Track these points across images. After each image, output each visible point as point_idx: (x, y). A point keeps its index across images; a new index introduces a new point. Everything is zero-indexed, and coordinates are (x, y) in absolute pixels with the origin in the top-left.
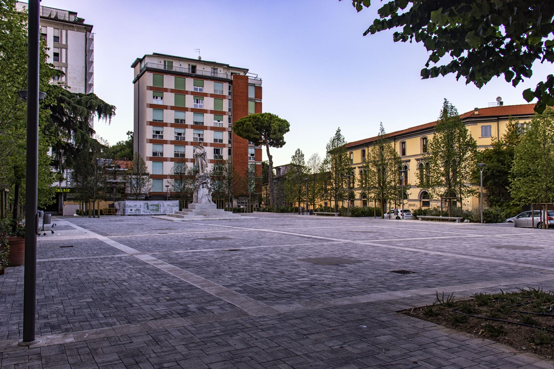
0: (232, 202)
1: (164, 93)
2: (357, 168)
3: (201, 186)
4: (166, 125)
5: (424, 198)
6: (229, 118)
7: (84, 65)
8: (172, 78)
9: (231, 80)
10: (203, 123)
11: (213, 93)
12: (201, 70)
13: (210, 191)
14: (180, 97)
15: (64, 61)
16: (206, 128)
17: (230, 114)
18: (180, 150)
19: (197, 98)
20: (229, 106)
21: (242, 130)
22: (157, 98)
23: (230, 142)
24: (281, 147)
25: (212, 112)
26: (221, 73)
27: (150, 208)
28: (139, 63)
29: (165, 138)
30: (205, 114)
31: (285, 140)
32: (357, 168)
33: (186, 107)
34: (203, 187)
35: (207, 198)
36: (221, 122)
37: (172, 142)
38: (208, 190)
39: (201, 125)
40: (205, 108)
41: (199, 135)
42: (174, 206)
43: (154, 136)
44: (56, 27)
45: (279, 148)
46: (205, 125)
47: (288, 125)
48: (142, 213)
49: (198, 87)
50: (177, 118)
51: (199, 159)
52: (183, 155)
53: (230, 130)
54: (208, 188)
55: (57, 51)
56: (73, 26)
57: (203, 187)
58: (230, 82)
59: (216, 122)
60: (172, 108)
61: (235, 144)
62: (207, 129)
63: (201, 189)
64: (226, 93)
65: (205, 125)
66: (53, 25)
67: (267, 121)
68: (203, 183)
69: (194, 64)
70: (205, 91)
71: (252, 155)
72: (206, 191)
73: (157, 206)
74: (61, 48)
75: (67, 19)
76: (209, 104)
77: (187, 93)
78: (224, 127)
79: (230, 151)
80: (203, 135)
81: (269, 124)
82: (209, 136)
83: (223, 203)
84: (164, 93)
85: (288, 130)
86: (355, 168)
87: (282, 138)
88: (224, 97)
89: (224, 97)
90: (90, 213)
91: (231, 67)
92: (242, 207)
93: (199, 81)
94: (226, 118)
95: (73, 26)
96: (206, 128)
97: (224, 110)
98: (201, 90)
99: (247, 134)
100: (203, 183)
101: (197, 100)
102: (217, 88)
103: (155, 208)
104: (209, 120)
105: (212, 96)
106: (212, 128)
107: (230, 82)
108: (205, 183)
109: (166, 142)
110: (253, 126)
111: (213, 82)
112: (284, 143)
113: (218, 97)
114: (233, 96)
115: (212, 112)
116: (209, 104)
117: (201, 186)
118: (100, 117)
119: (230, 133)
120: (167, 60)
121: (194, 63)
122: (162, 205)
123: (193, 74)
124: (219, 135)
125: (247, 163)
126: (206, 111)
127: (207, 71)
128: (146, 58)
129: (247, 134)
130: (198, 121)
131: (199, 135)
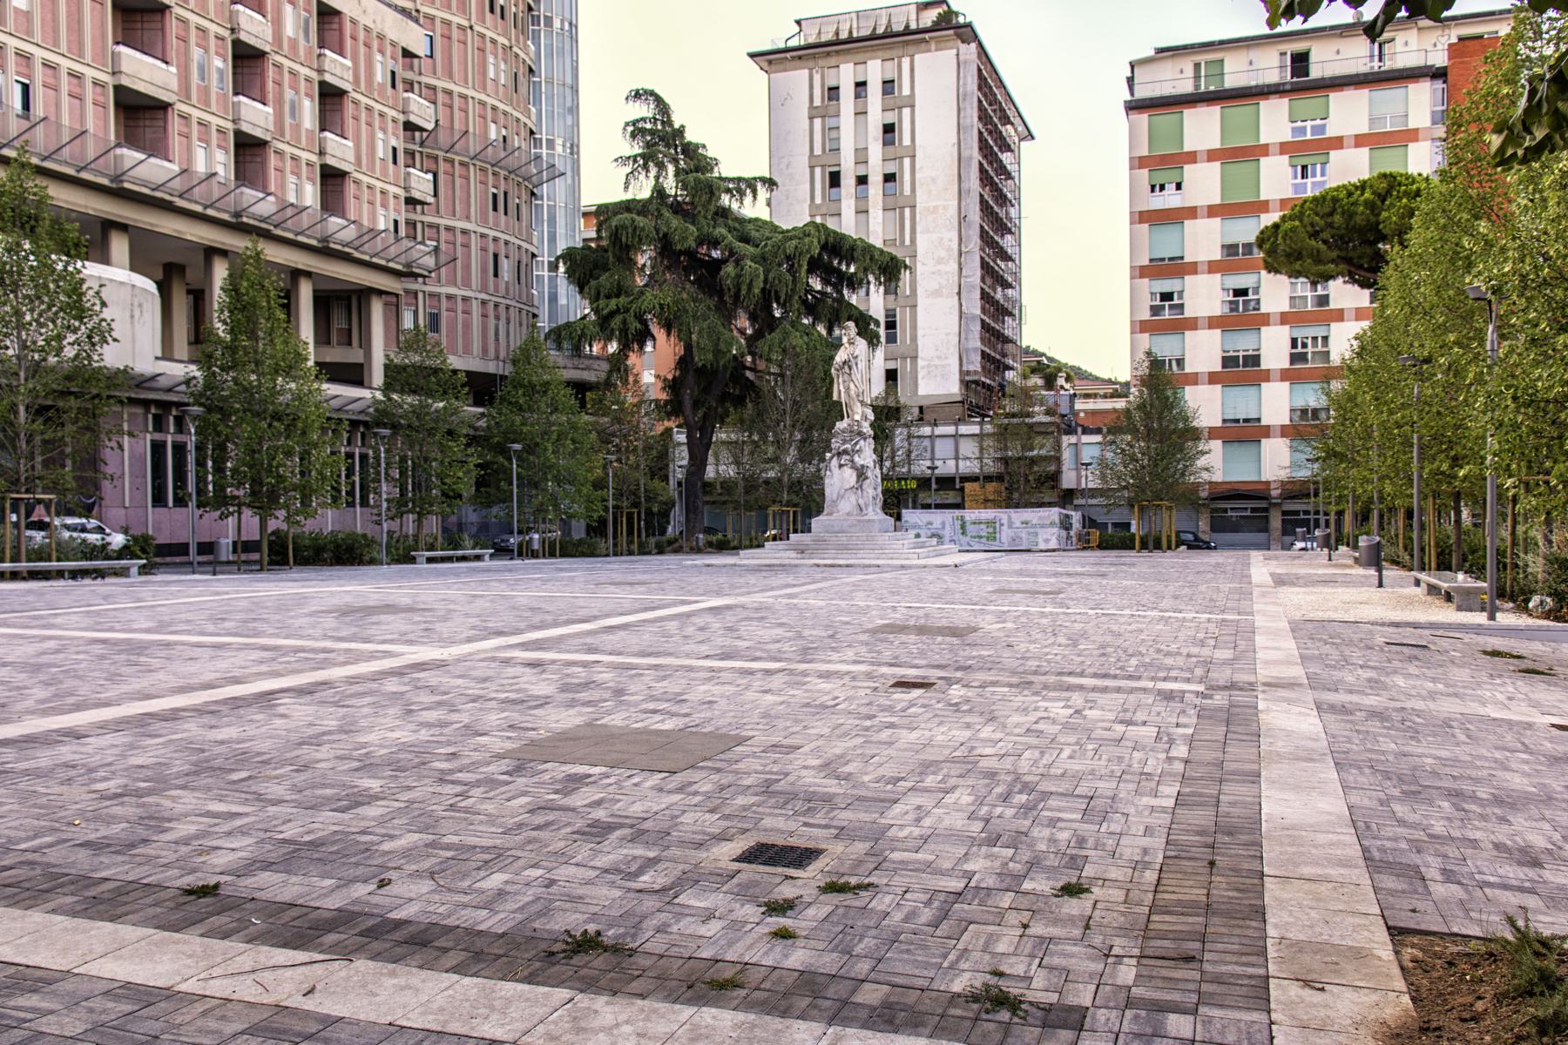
1: (1186, 167)
4: (1193, 269)
7: (955, 140)
8: (1213, 113)
14: (1241, 169)
15: (907, 141)
18: (1242, 343)
19: (1304, 161)
22: (1162, 188)
29: (1189, 313)
34: (841, 466)
35: (853, 499)
37: (1213, 323)
42: (1043, 526)
43: (1155, 310)
44: (888, 54)
50: (1229, 241)
52: (1254, 360)
55: (891, 118)
56: (924, 40)
57: (841, 466)
58: (1439, 74)
60: (1213, 211)
63: (836, 470)
66: (880, 54)
69: (1299, 46)
74: (900, 108)
75: (913, 26)
77: (1264, 150)
84: (1186, 167)
90: (225, 553)
95: (924, 40)
98: (1322, 129)
101: (1304, 168)
108: (846, 452)
109: (1192, 324)
120: (1202, 58)
122: (1005, 521)
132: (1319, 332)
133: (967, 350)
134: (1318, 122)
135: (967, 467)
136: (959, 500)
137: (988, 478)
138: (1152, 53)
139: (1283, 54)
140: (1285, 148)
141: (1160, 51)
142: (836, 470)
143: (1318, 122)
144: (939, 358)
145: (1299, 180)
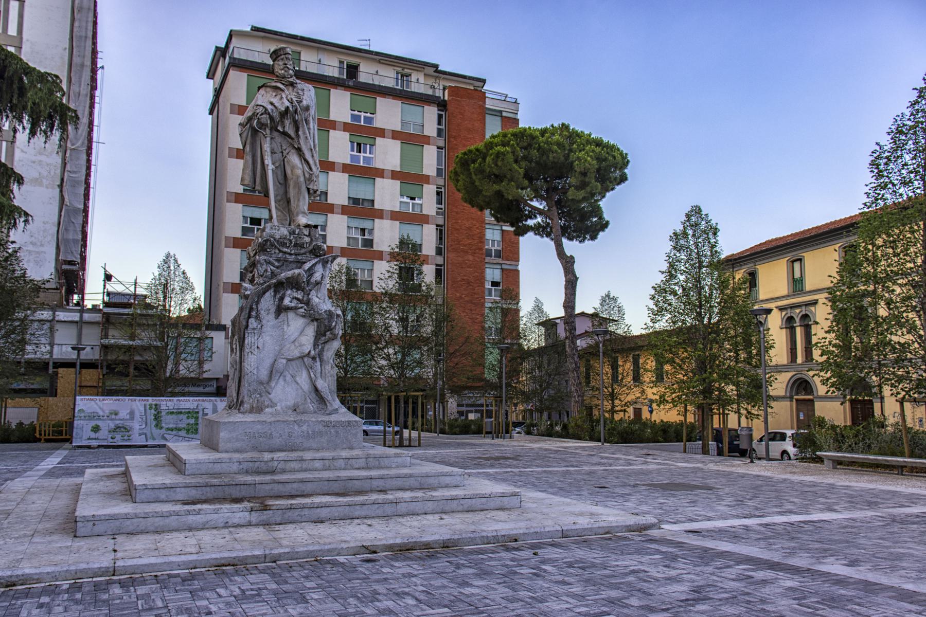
0: (443, 401)
2: (775, 312)
3: (268, 302)
5: (797, 394)
6: (438, 193)
9: (444, 101)
10: (373, 201)
11: (399, 129)
12: (367, 73)
13: (323, 332)
16: (380, 214)
17: (441, 182)
20: (439, 163)
21: (481, 171)
23: (439, 252)
24: (593, 238)
25: (395, 175)
26: (419, 84)
27: (169, 421)
28: (221, 59)
30: (378, 179)
31: (606, 216)
32: (775, 312)
33: (330, 160)
34: (281, 310)
35: (303, 379)
36: (417, 201)
38: (311, 331)
39: (366, 205)
40: (378, 164)
41: (363, 231)
43: (245, 231)
45: (588, 243)
46: (376, 206)
47: (624, 162)
48: (139, 440)
49: (363, 114)
51: (267, 147)
53: (441, 222)
54: (312, 316)
57: (281, 310)
59: (405, 199)
61: (452, 255)
62: (382, 218)
63: (269, 319)
64: (431, 129)
65: (376, 206)
67: (559, 144)
68: (280, 286)
69: (353, 60)
70: (378, 123)
71: (495, 284)
72: (298, 333)
73: (193, 414)
76: (388, 155)
78: (425, 212)
79: (439, 273)
80: (371, 231)
81: (567, 157)
82: (386, 235)
83: (415, 403)
85: (623, 179)
86: (769, 311)
87: (597, 211)
88: (426, 140)
89: (426, 140)
91: (444, 73)
92: (471, 416)
93: (364, 100)
94: (429, 191)
96: (380, 214)
97: (425, 172)
99: (496, 187)
100: (280, 286)
101: (359, 145)
102: (408, 118)
103: (185, 422)
104: (387, 195)
105: (395, 135)
106: (395, 216)
107: (442, 105)
108: (294, 283)
110: (516, 161)
111: (398, 103)
112: (604, 226)
113: (411, 140)
114: (448, 141)
115: (395, 175)
116: (388, 155)
117: (268, 302)
118: (33, 133)
119: (440, 230)
121: (353, 59)
123: (350, 80)
124: (413, 233)
125: (483, 305)
126: (380, 173)
127: (387, 77)
128: (235, 42)
129: (496, 187)
130: (361, 196)
131: (363, 231)
132: (367, 265)
133: (67, 241)
134: (368, 115)
135: (63, 352)
136: (46, 385)
137: (87, 365)
138: (249, 29)
139: (341, 62)
140: (346, 127)
141: (255, 29)
142: (269, 319)
143: (368, 115)
144: (32, 243)
145: (355, 153)
